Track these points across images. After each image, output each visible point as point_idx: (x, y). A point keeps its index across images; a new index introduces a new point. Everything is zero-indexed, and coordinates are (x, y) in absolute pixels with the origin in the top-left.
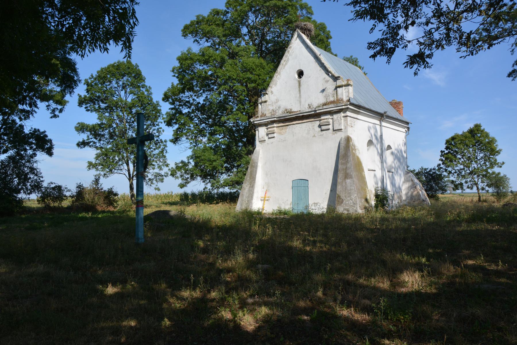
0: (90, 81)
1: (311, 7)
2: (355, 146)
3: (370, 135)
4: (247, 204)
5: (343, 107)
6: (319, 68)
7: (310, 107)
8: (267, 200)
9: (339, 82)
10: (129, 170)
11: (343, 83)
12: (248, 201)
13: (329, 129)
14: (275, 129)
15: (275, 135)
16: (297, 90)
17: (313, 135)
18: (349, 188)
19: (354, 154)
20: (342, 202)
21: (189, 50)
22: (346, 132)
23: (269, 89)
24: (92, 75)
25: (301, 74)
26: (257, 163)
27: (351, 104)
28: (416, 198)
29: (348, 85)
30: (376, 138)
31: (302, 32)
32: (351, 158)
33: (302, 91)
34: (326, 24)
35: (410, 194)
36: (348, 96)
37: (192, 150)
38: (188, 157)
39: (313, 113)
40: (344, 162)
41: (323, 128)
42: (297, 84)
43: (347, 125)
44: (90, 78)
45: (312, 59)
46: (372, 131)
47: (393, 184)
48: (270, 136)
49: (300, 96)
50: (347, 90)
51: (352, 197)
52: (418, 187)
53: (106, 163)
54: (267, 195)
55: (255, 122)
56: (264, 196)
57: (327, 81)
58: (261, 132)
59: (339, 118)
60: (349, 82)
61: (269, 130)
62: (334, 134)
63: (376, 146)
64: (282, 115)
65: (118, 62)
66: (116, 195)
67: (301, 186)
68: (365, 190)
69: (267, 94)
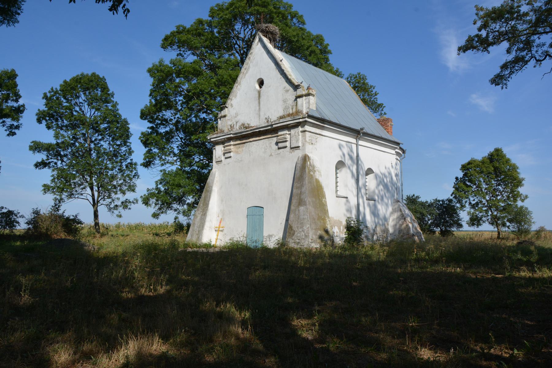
0: (49, 95)
1: (302, 16)
2: (314, 167)
3: (341, 153)
4: (197, 234)
5: (301, 120)
6: (279, 76)
7: (268, 121)
8: (222, 231)
9: (300, 92)
10: (93, 195)
11: (304, 93)
12: (199, 231)
13: (286, 147)
14: (232, 147)
16: (257, 102)
17: (270, 154)
18: (302, 217)
19: (311, 177)
20: (293, 234)
21: (161, 62)
22: (304, 149)
23: (229, 102)
24: (52, 89)
25: (261, 83)
26: (212, 187)
27: (310, 116)
28: (405, 232)
29: (308, 95)
30: (351, 158)
31: (264, 36)
32: (306, 181)
33: (262, 103)
34: (323, 36)
35: (398, 226)
36: (309, 108)
37: (162, 173)
38: (156, 182)
39: (270, 127)
40: (298, 185)
41: (281, 145)
43: (306, 141)
44: (50, 92)
45: (272, 65)
46: (346, 150)
47: (375, 213)
48: (227, 155)
49: (259, 109)
50: (307, 100)
51: (305, 228)
52: (409, 219)
53: (63, 185)
54: (222, 225)
55: (212, 140)
56: (218, 226)
57: (287, 91)
58: (218, 151)
59: (297, 134)
60: (311, 92)
61: (226, 148)
62: (291, 152)
63: (349, 168)
64: (238, 131)
65: (81, 75)
66: (80, 222)
67: (256, 214)
68: (324, 219)
69: (227, 107)
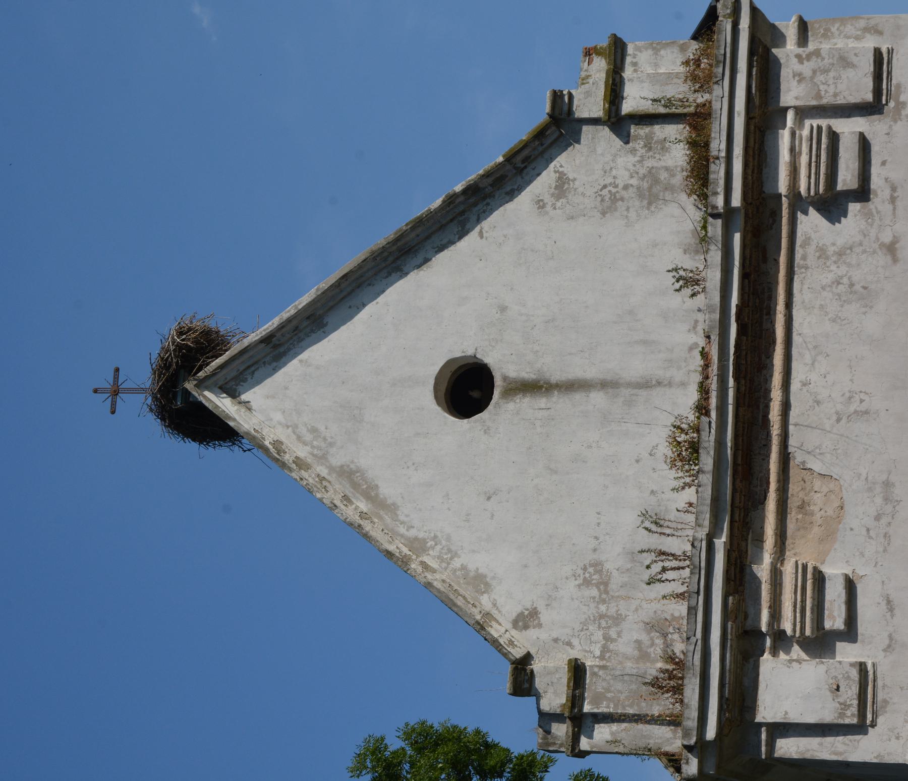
9: (589, 102)
15: (834, 571)
16: (559, 403)
17: (882, 259)
25: (467, 389)
33: (578, 370)
39: (737, 237)
42: (525, 404)
49: (604, 385)
57: (562, 185)
59: (806, 69)
